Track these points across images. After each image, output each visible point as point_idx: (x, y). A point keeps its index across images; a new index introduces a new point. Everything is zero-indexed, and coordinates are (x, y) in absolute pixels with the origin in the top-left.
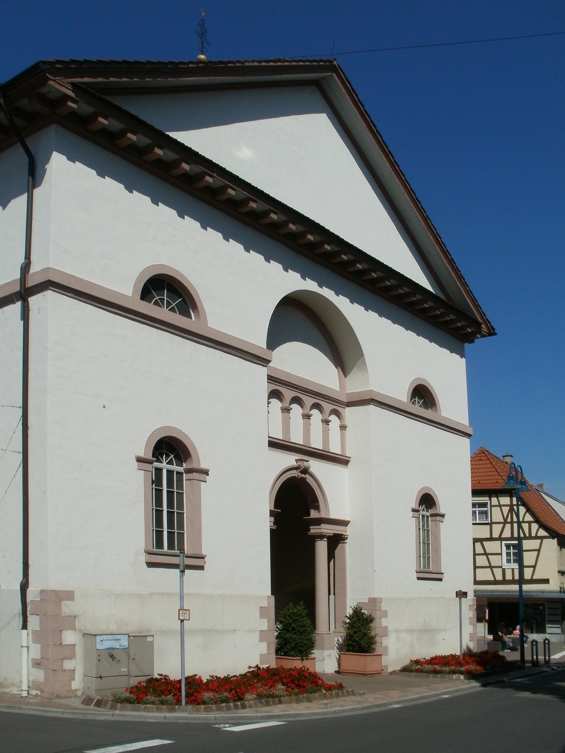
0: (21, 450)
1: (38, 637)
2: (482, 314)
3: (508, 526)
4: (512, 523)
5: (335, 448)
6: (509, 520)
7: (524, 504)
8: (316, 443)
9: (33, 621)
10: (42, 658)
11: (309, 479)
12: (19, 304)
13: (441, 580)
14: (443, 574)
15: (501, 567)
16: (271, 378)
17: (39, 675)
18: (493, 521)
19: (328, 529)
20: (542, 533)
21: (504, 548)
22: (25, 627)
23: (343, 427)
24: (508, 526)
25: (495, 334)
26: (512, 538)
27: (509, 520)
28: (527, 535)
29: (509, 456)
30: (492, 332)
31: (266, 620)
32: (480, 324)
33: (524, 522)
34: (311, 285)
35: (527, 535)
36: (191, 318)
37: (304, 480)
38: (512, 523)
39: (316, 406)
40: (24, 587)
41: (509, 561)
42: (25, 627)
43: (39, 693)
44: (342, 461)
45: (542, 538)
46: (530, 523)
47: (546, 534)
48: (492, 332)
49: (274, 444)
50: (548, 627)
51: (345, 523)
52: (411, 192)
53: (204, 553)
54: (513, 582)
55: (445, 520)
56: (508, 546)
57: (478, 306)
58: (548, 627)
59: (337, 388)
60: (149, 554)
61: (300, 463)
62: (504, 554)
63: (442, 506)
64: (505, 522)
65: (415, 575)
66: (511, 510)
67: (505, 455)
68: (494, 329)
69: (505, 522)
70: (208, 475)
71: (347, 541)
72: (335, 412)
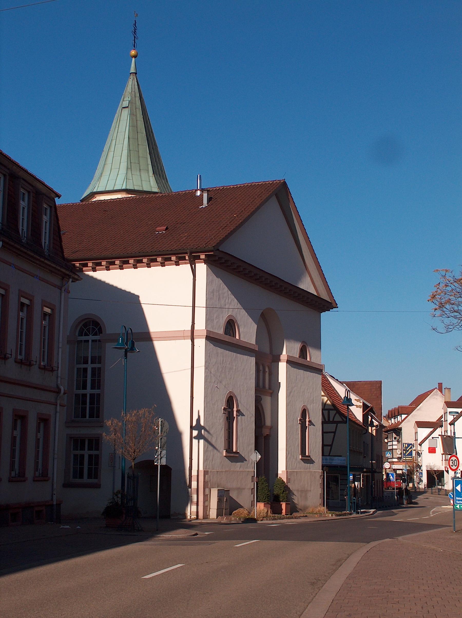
28: (327, 420)
35: (327, 420)
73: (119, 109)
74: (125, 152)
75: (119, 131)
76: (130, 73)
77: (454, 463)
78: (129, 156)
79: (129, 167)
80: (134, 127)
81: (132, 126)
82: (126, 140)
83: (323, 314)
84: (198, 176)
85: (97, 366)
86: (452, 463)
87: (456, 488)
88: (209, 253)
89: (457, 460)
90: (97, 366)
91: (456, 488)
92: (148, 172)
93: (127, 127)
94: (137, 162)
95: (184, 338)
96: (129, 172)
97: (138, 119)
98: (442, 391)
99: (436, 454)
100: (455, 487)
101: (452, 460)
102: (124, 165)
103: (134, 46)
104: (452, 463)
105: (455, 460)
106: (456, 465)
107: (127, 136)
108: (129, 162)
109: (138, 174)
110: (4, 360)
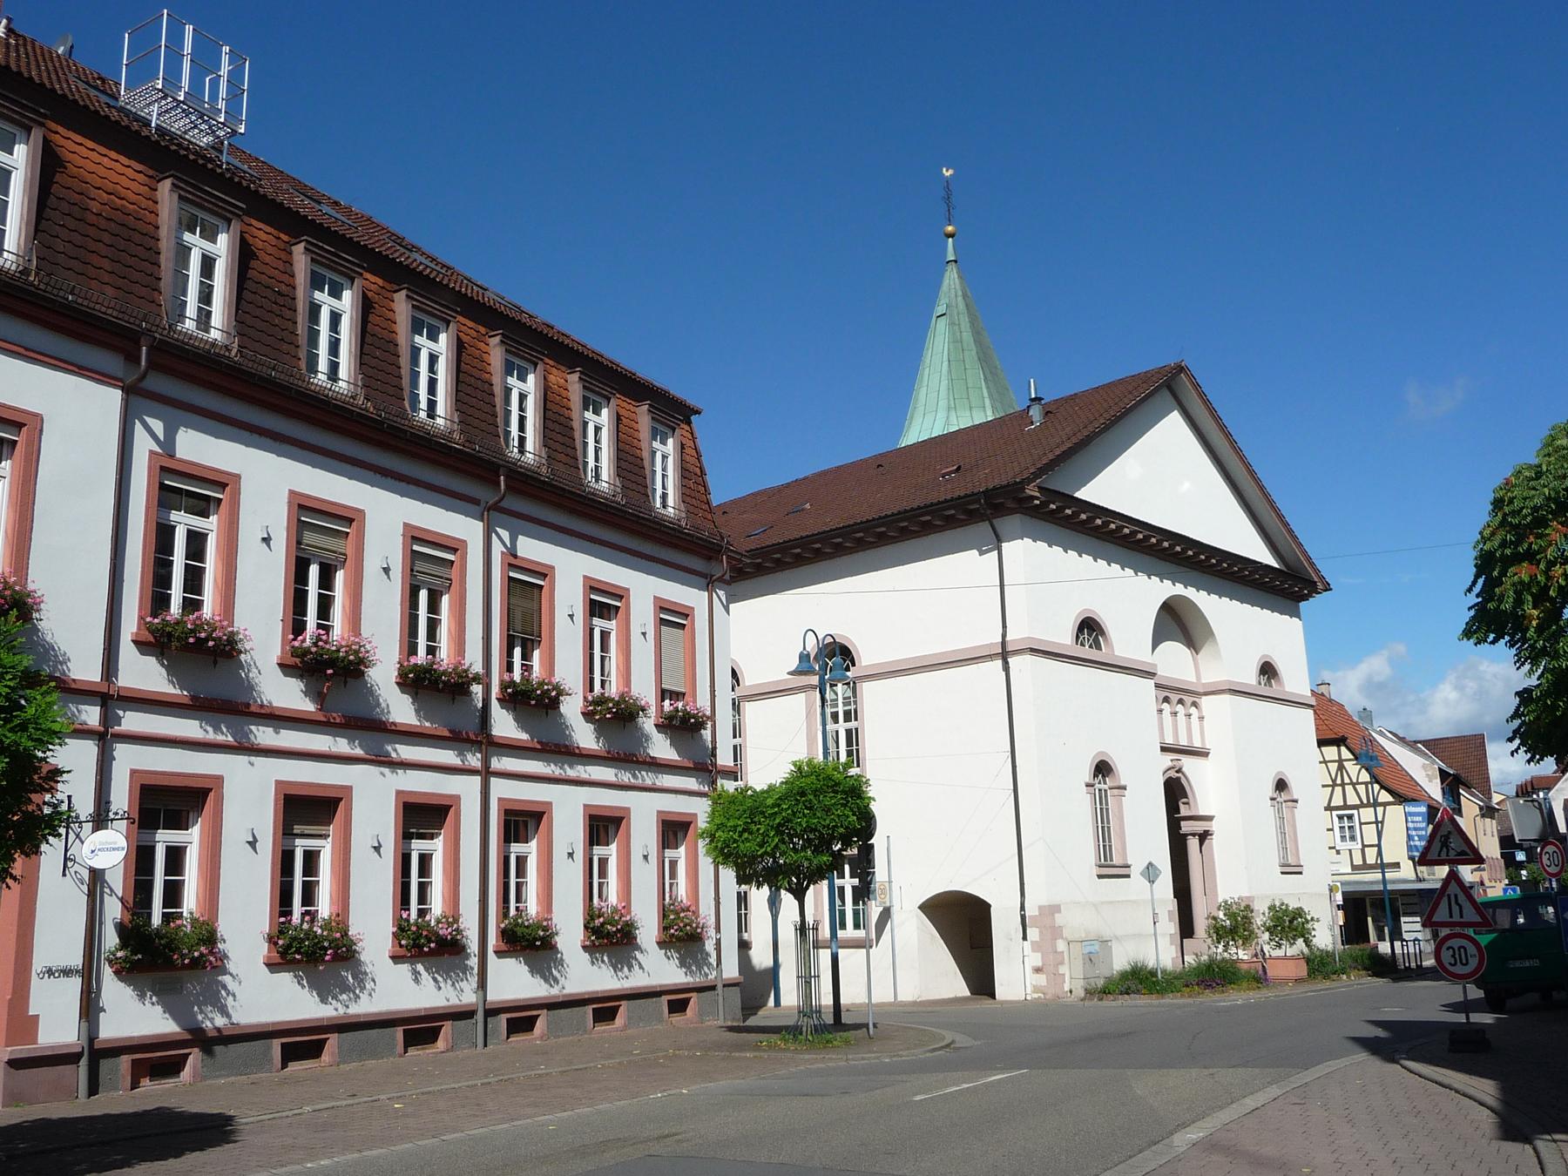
0: (1012, 788)
1: (1036, 947)
2: (1317, 571)
3: (1338, 790)
4: (1343, 785)
5: (1197, 743)
6: (1339, 781)
7: (1378, 782)
8: (1183, 742)
9: (1033, 933)
10: (1043, 965)
11: (1183, 781)
12: (1332, 805)
13: (1301, 873)
14: (1129, 867)
15: (1334, 848)
16: (1157, 686)
17: (1042, 980)
18: (1348, 804)
19: (1199, 827)
20: (1385, 797)
21: (1336, 820)
22: (1025, 938)
23: (1201, 718)
24: (1338, 790)
25: (1331, 589)
26: (1345, 807)
27: (1339, 781)
28: (1365, 802)
29: (1325, 684)
30: (1327, 588)
31: (1172, 923)
32: (1316, 582)
33: (1358, 783)
34: (1180, 589)
35: (1365, 802)
36: (1101, 650)
37: (1179, 779)
38: (1343, 785)
39: (1181, 702)
40: (1022, 908)
41: (1343, 838)
42: (1025, 938)
43: (1042, 996)
44: (1202, 753)
45: (1385, 805)
46: (1366, 784)
47: (1391, 799)
48: (1327, 588)
49: (1164, 749)
50: (1405, 923)
51: (1209, 818)
52: (1248, 466)
53: (1129, 863)
54: (1372, 867)
55: (1298, 805)
56: (1340, 818)
57: (1312, 564)
58: (1405, 923)
59: (1194, 680)
60: (1100, 867)
61: (1175, 763)
62: (1337, 830)
63: (1296, 789)
64: (1334, 785)
65: (1279, 870)
66: (1341, 768)
67: (1320, 683)
68: (1329, 585)
69: (1334, 785)
70: (1125, 789)
71: (1214, 837)
72: (1194, 704)
73: (934, 318)
74: (945, 383)
75: (934, 353)
76: (948, 262)
77: (1551, 859)
78: (951, 389)
79: (953, 406)
80: (957, 342)
81: (954, 342)
82: (946, 364)
83: (1301, 604)
84: (1030, 382)
85: (852, 725)
86: (1549, 859)
87: (1565, 916)
88: (226, 195)
89: (1558, 851)
90: (852, 725)
91: (1565, 916)
92: (985, 411)
93: (946, 345)
94: (965, 396)
95: (990, 657)
96: (953, 413)
97: (963, 329)
98: (363, 297)
99: (225, 776)
100: (1562, 914)
101: (1547, 853)
102: (943, 403)
103: (949, 220)
104: (1549, 859)
105: (1555, 852)
106: (1557, 863)
107: (945, 358)
108: (951, 398)
109: (968, 413)
110: (622, 723)
